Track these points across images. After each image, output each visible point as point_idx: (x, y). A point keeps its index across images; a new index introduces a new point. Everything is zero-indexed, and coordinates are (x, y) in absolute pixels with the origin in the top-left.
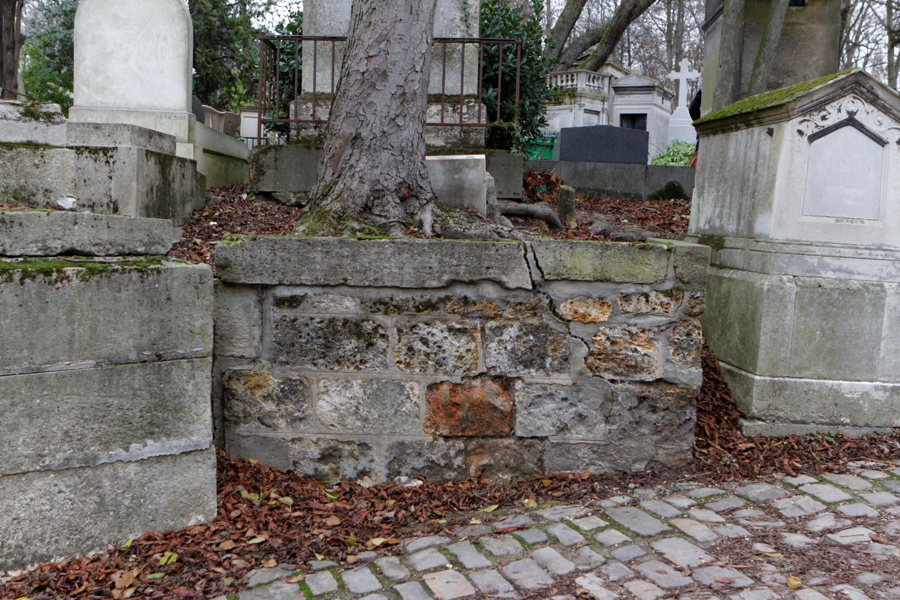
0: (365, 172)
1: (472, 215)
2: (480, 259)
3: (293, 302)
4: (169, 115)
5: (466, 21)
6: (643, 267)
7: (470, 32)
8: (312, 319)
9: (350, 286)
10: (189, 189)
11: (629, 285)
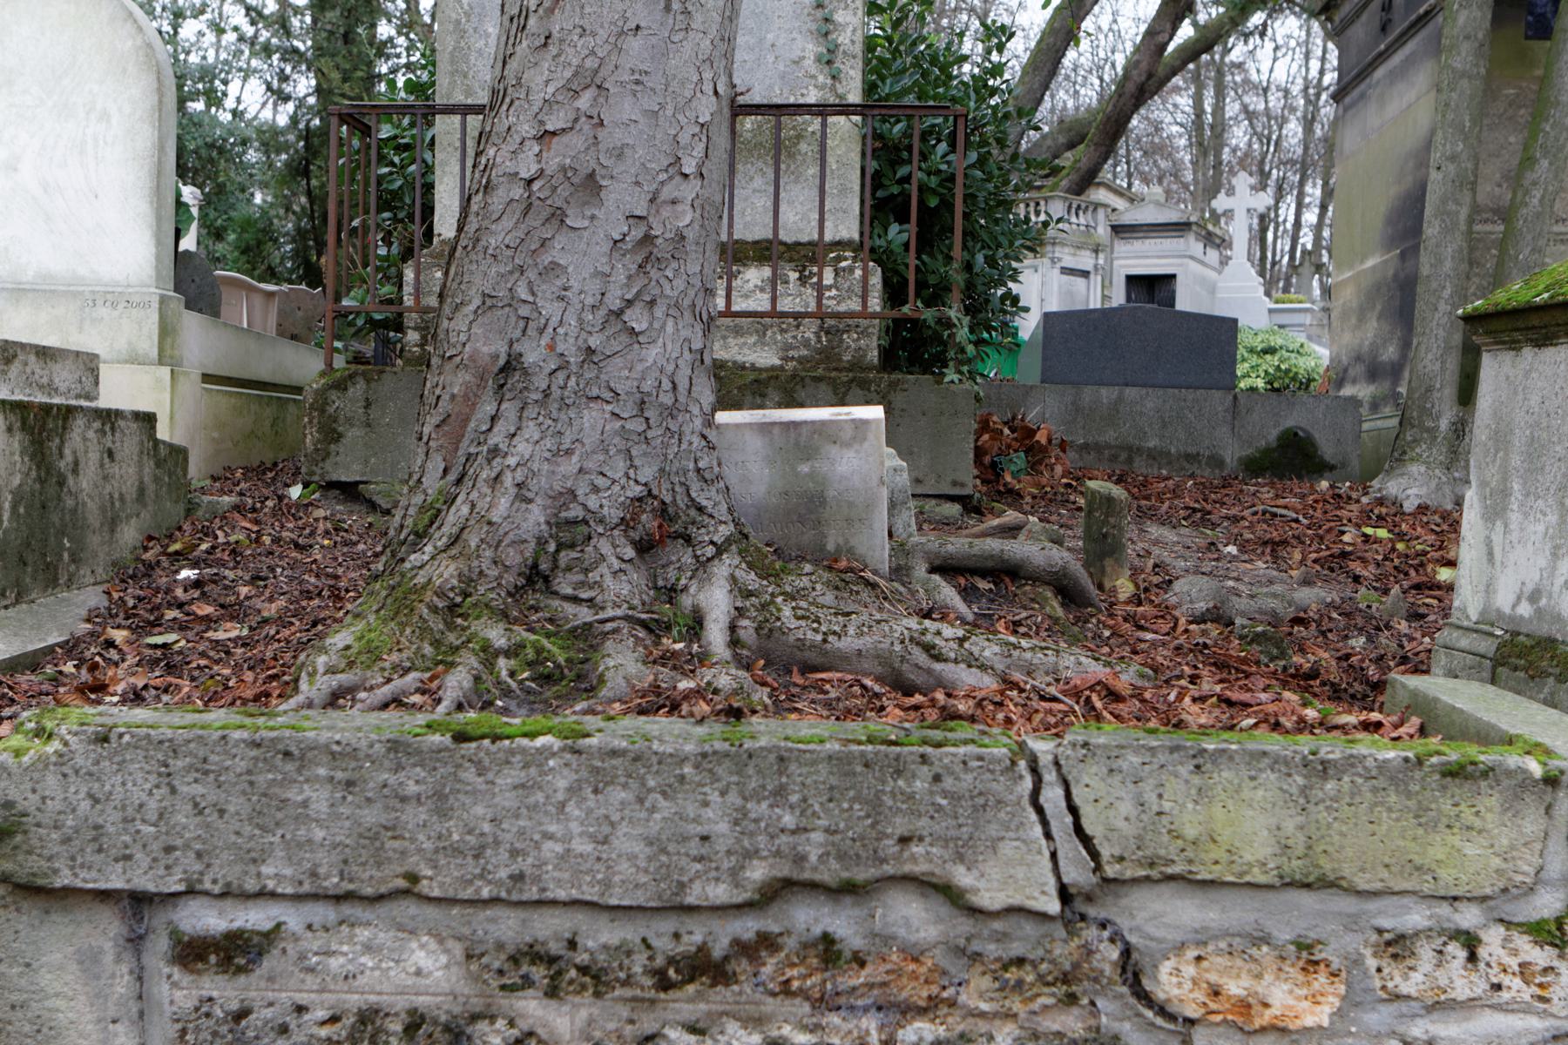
0: (536, 469)
1: (848, 574)
2: (875, 807)
3: (236, 952)
4: (94, 298)
5: (829, 62)
6: (1456, 840)
7: (840, 91)
8: (300, 1009)
9: (430, 899)
10: (130, 489)
11: (1406, 900)
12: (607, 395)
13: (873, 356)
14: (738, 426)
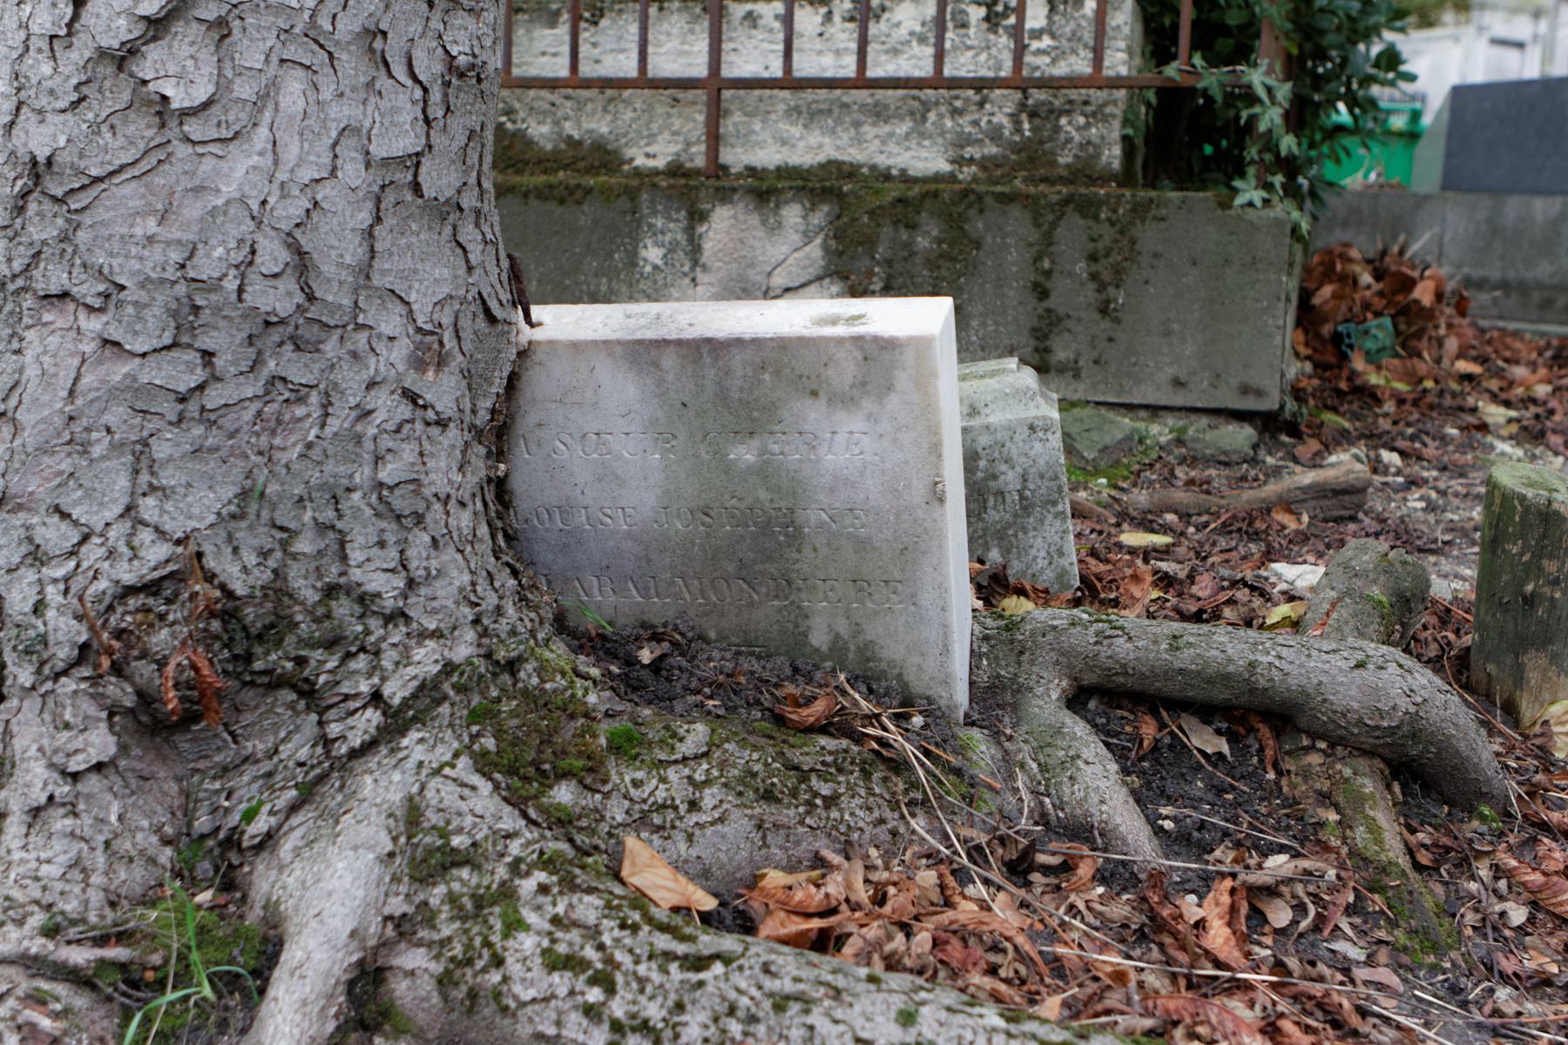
12: (89, 290)
13: (1113, 156)
14: (577, 347)
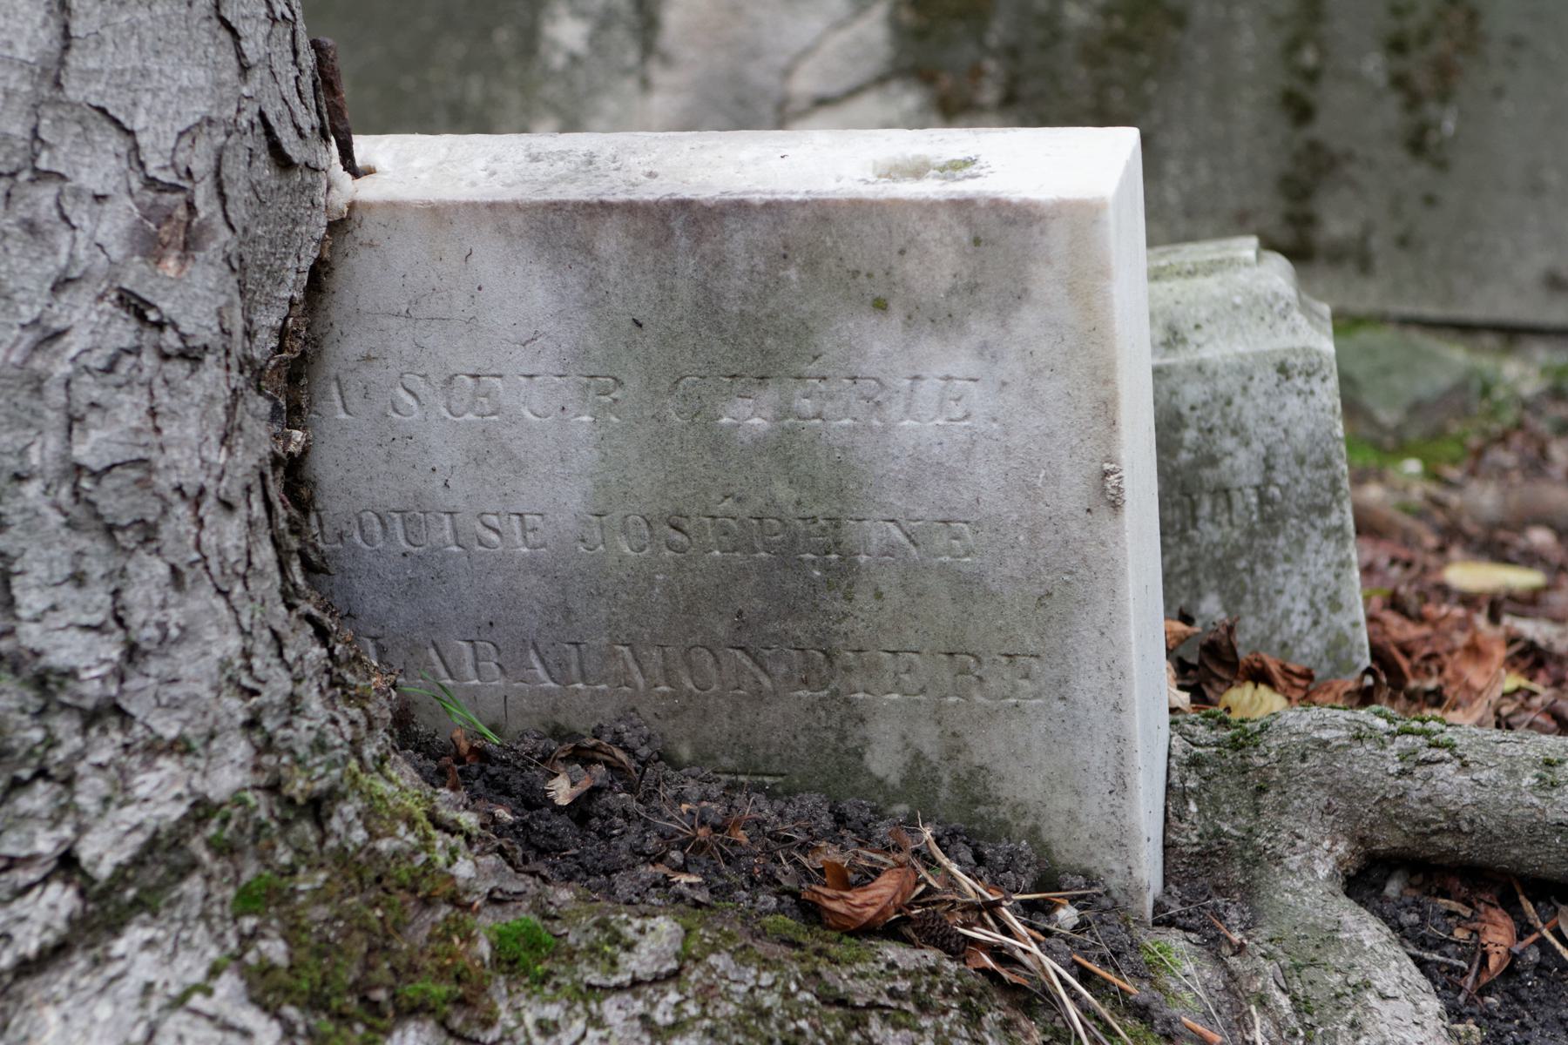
14: (438, 214)
